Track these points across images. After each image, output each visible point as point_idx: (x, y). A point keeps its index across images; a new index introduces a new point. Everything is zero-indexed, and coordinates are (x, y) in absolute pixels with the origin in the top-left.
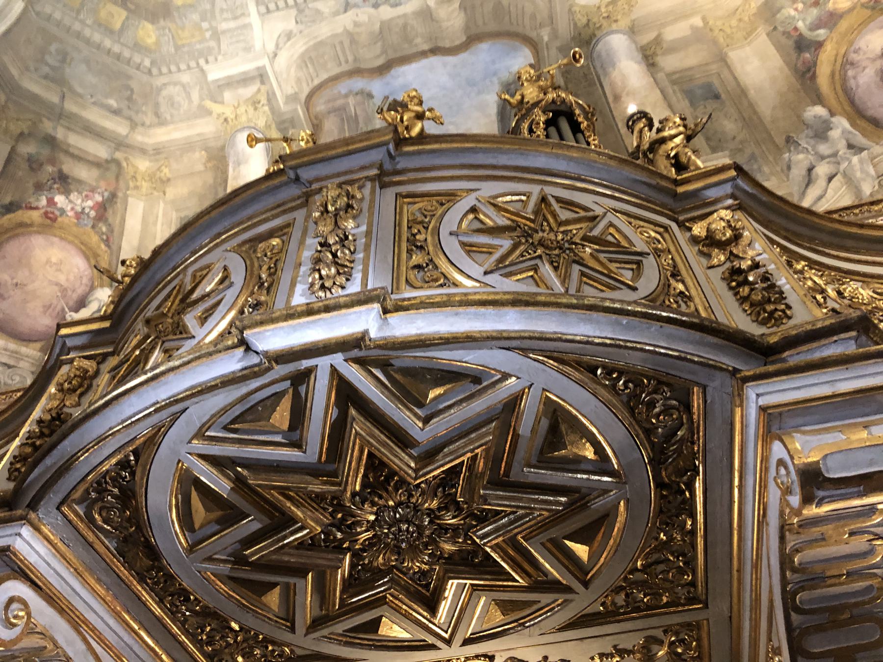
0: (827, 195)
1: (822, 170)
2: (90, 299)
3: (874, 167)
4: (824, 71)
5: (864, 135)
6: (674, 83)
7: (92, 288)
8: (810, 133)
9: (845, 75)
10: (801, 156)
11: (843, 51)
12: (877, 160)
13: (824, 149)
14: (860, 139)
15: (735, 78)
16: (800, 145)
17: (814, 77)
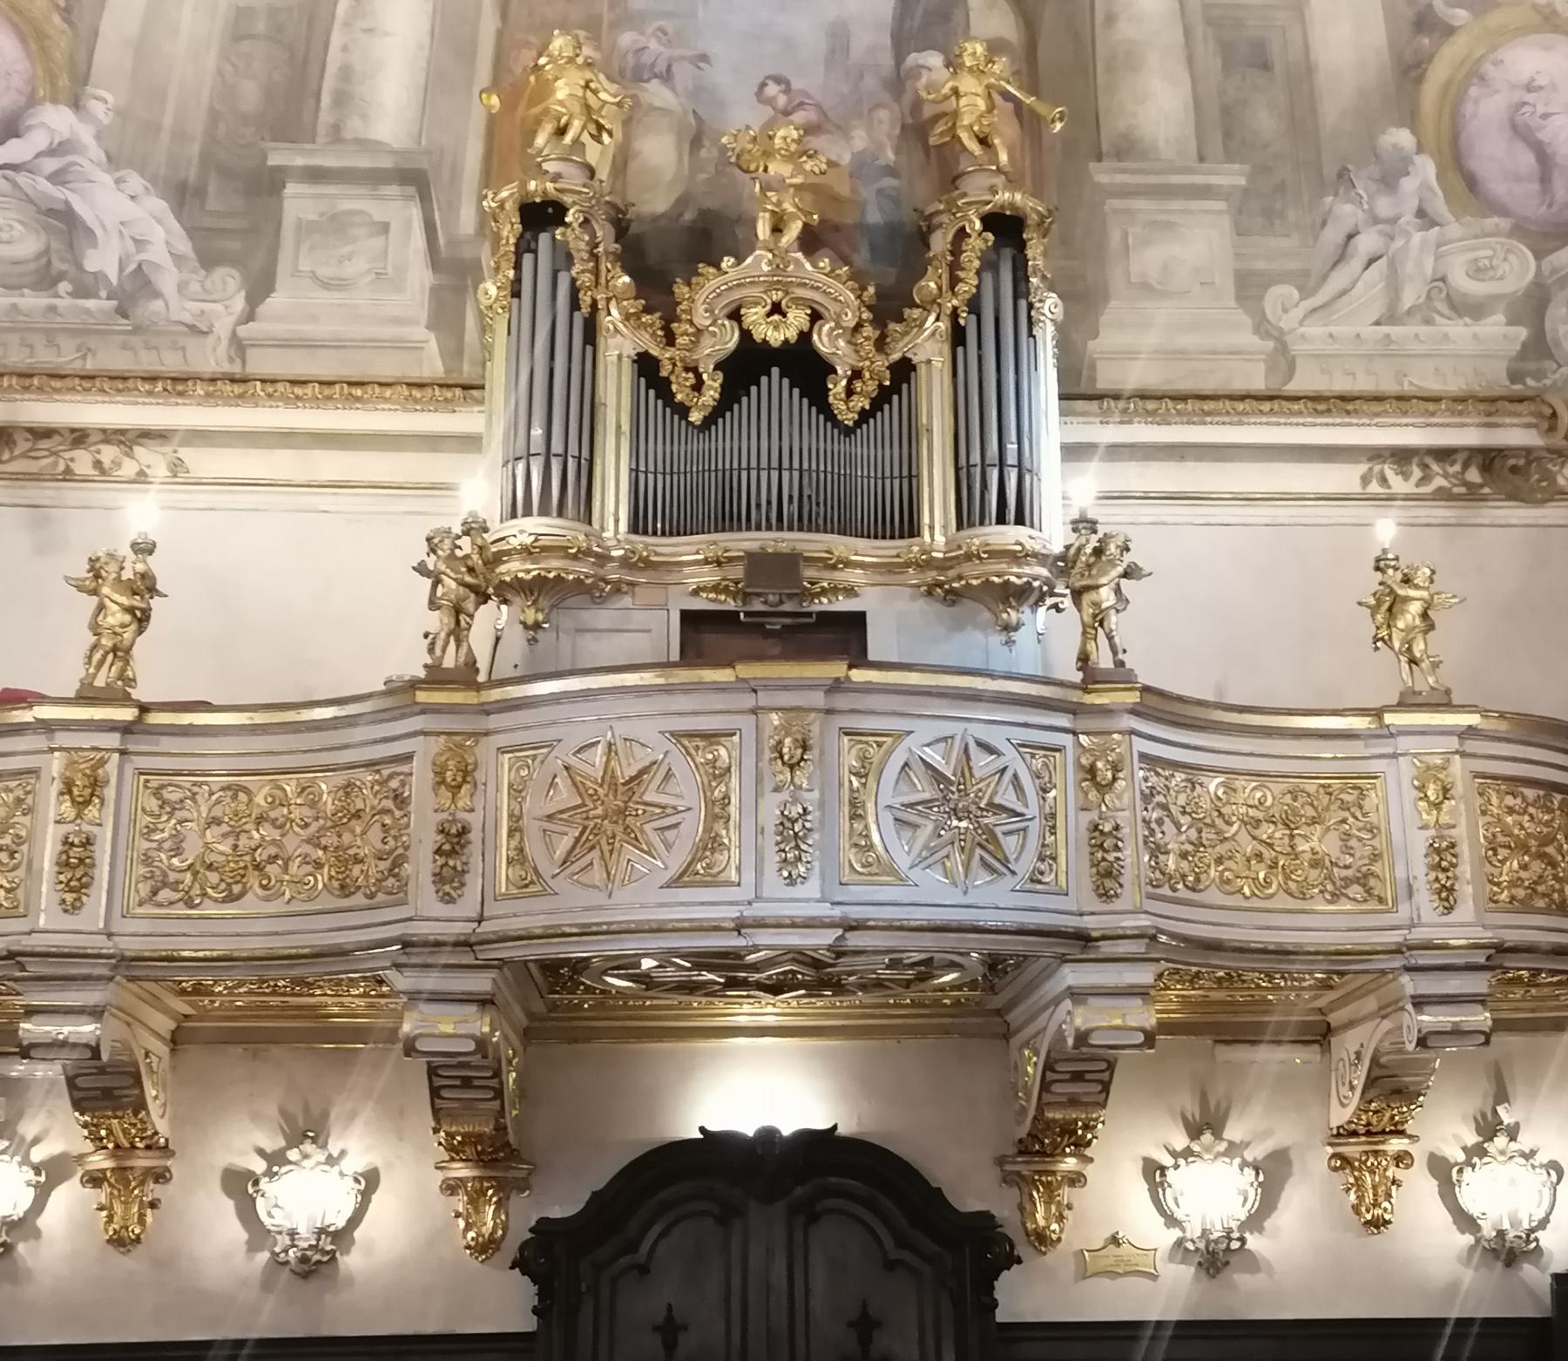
0: (1352, 292)
1: (1367, 242)
2: (28, 123)
3: (1436, 259)
4: (1430, 90)
5: (1448, 201)
6: (1210, 22)
7: (32, 101)
8: (1375, 170)
9: (1466, 91)
10: (1348, 208)
11: (1477, 54)
12: (1445, 248)
13: (1384, 206)
14: (1439, 206)
15: (1306, 46)
16: (1354, 187)
17: (1419, 80)
